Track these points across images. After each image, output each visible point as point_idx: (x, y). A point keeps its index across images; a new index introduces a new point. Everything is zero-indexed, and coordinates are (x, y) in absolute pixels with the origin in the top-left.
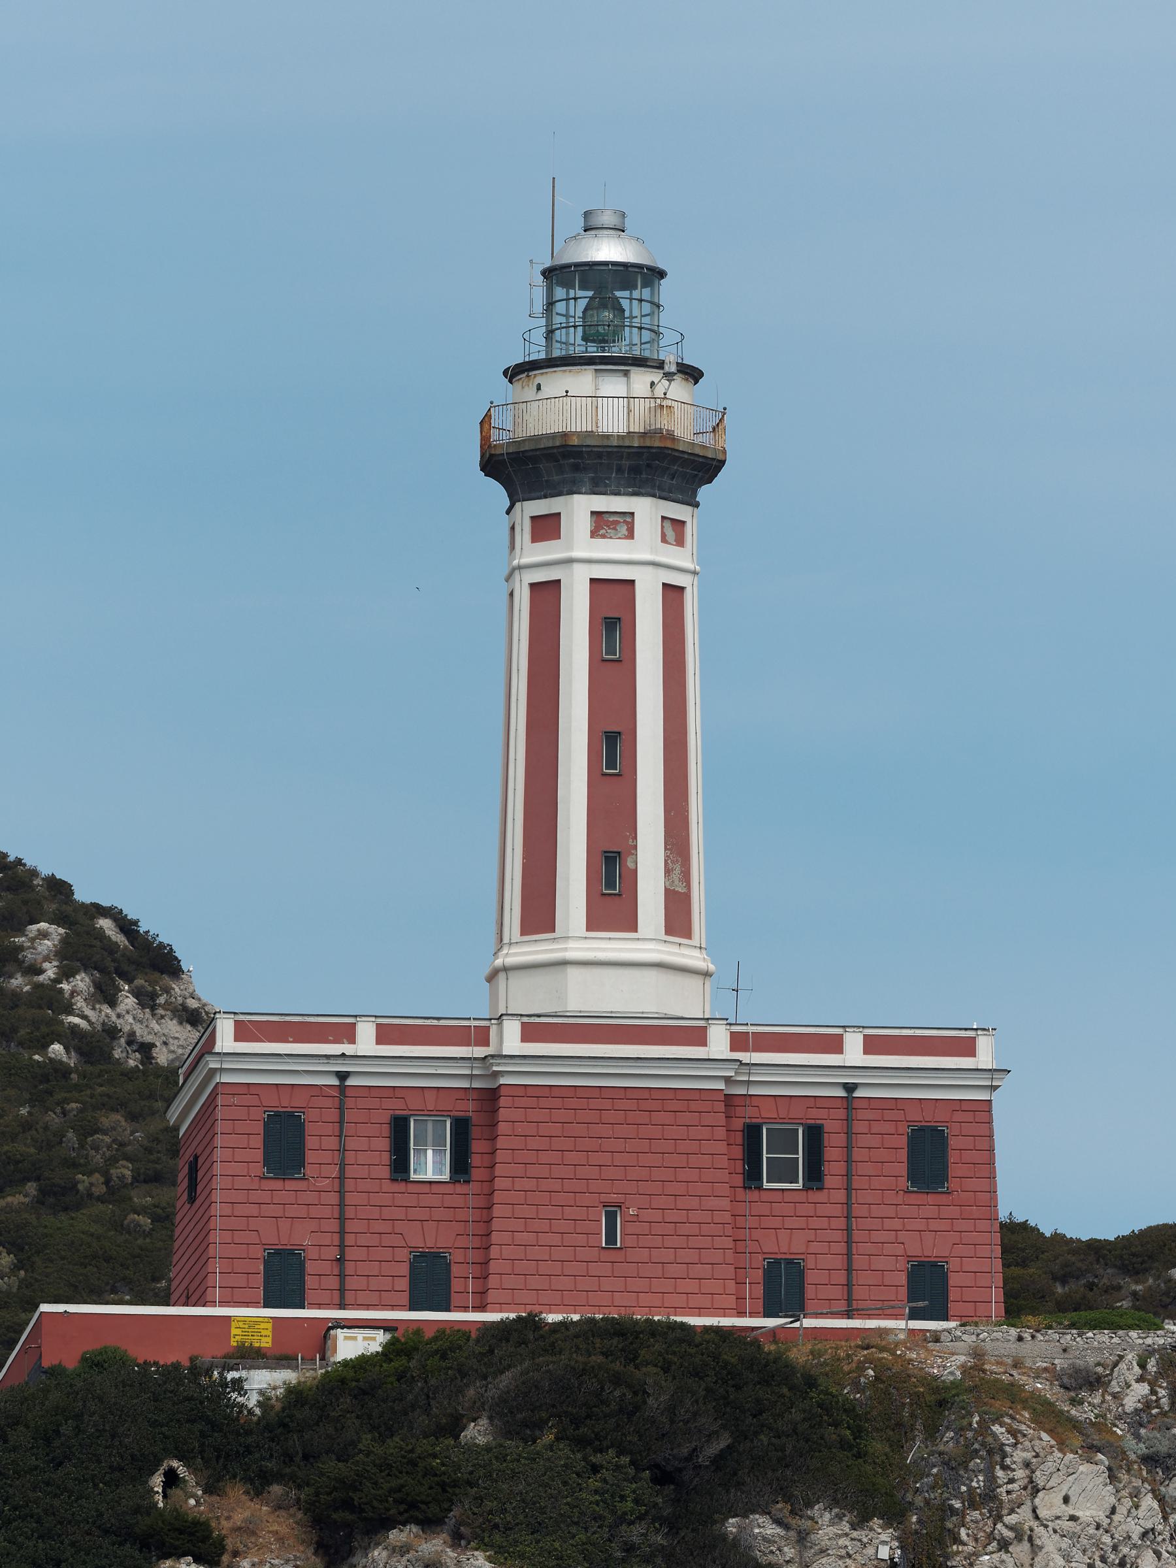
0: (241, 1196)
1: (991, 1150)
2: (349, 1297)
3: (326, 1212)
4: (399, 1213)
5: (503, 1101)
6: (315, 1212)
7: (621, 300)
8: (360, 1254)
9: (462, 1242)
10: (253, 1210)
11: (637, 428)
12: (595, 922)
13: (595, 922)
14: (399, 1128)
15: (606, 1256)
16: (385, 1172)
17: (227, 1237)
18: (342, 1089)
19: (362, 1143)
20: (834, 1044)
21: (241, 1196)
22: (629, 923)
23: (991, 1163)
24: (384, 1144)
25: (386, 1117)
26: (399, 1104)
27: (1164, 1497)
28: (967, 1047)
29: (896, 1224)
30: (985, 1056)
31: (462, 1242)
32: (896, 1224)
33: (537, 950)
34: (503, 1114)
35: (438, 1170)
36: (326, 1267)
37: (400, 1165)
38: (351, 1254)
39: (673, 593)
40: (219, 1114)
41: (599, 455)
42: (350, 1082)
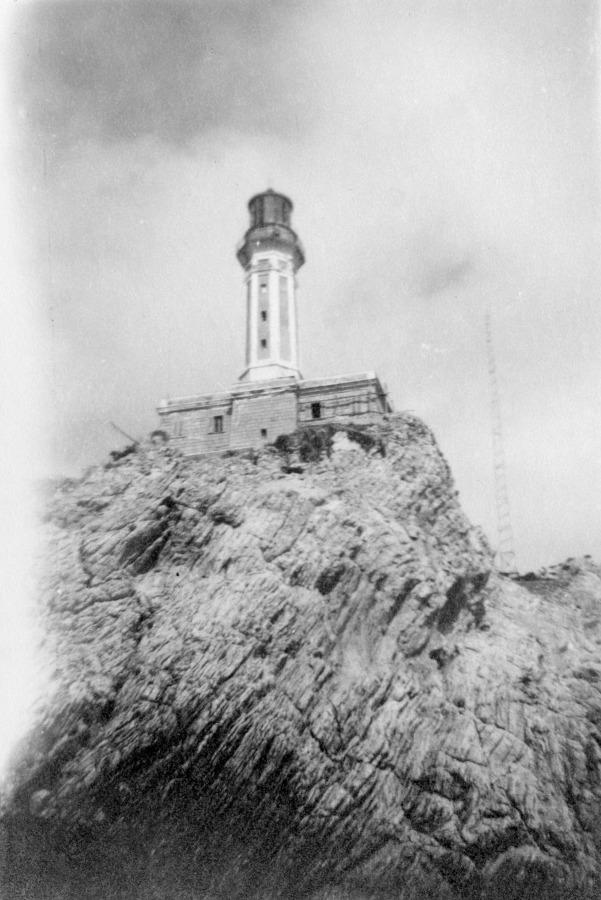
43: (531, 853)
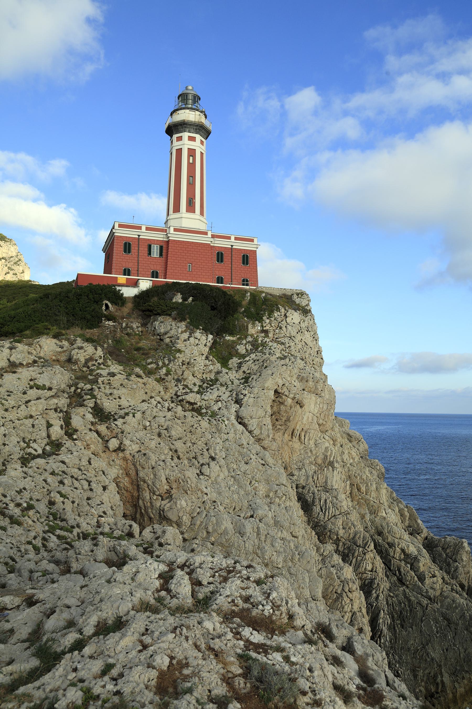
0: (119, 257)
1: (256, 259)
2: (139, 275)
3: (135, 261)
4: (149, 263)
5: (170, 242)
6: (133, 261)
7: (71, 654)
8: (142, 270)
9: (161, 269)
10: (121, 260)
11: (197, 120)
12: (188, 211)
13: (188, 211)
14: (150, 247)
15: (189, 273)
16: (147, 255)
17: (116, 259)
18: (139, 238)
19: (142, 249)
20: (229, 238)
21: (119, 257)
22: (194, 212)
23: (256, 262)
24: (147, 249)
25: (147, 244)
26: (150, 242)
27: (148, 603)
28: (252, 241)
29: (240, 271)
30: (256, 241)
31: (161, 269)
32: (240, 271)
33: (177, 215)
34: (170, 245)
35: (157, 255)
36: (135, 272)
37: (150, 254)
38: (140, 270)
39: (202, 154)
40: (115, 244)
41: (190, 125)
42: (140, 237)
43: (57, 590)
